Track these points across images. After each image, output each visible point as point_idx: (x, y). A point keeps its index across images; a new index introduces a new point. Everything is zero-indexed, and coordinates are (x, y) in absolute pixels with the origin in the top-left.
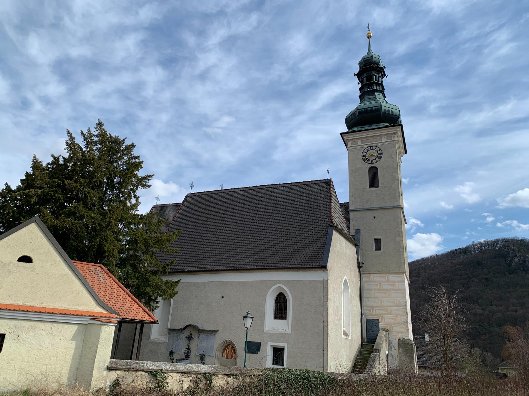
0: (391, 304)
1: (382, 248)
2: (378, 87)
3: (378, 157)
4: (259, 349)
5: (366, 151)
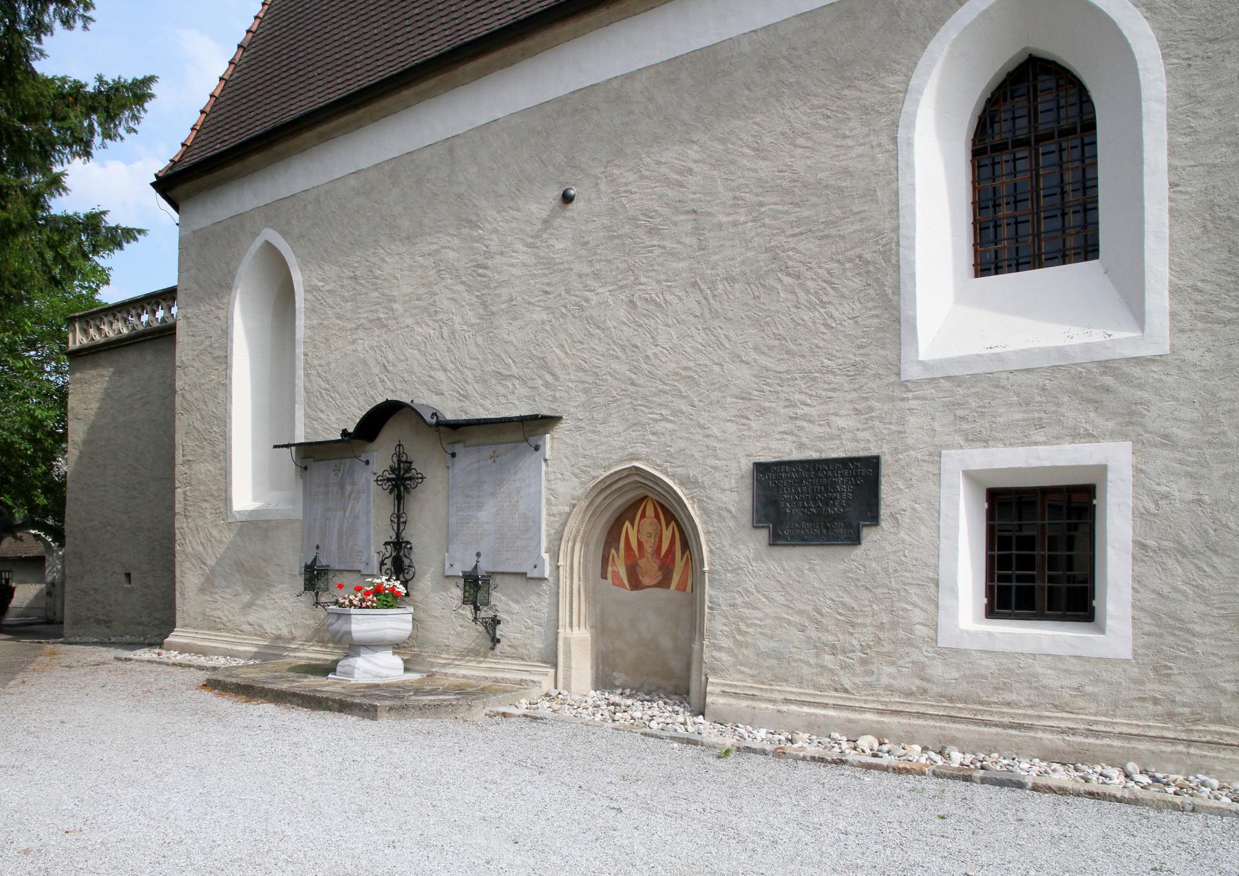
4: (869, 510)
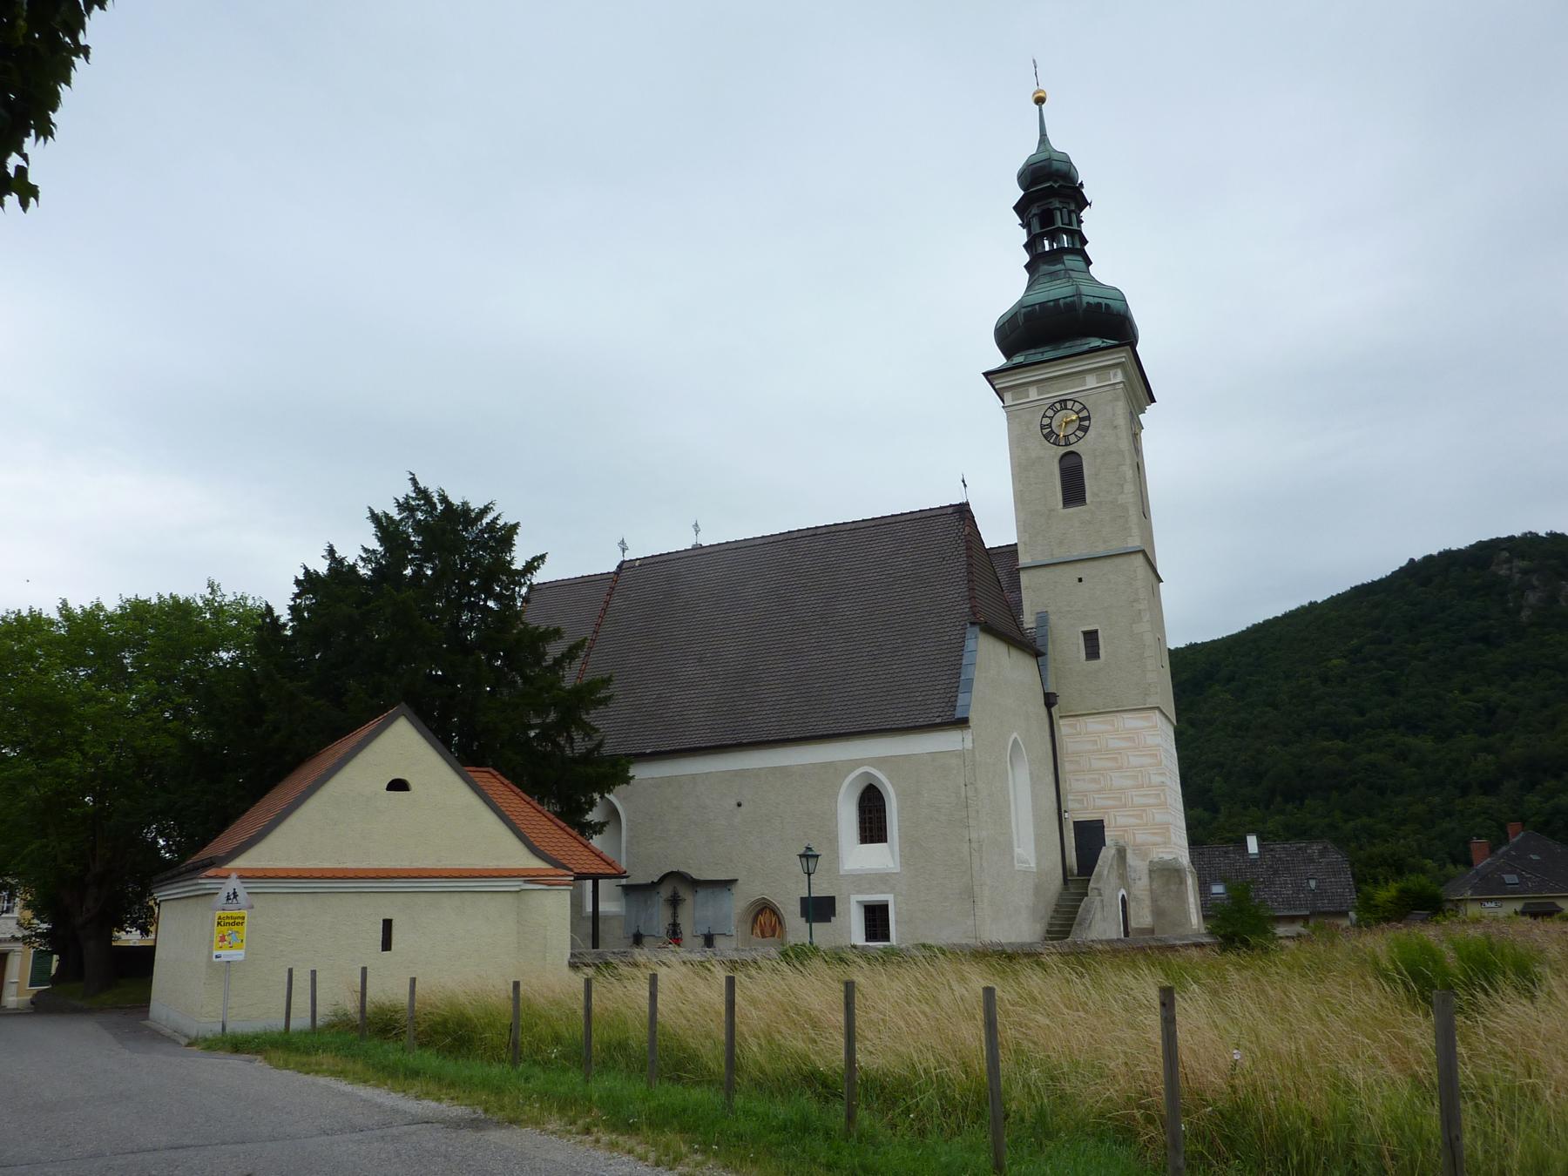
0: (1129, 783)
1: (1102, 652)
3: (1080, 428)
5: (1050, 413)
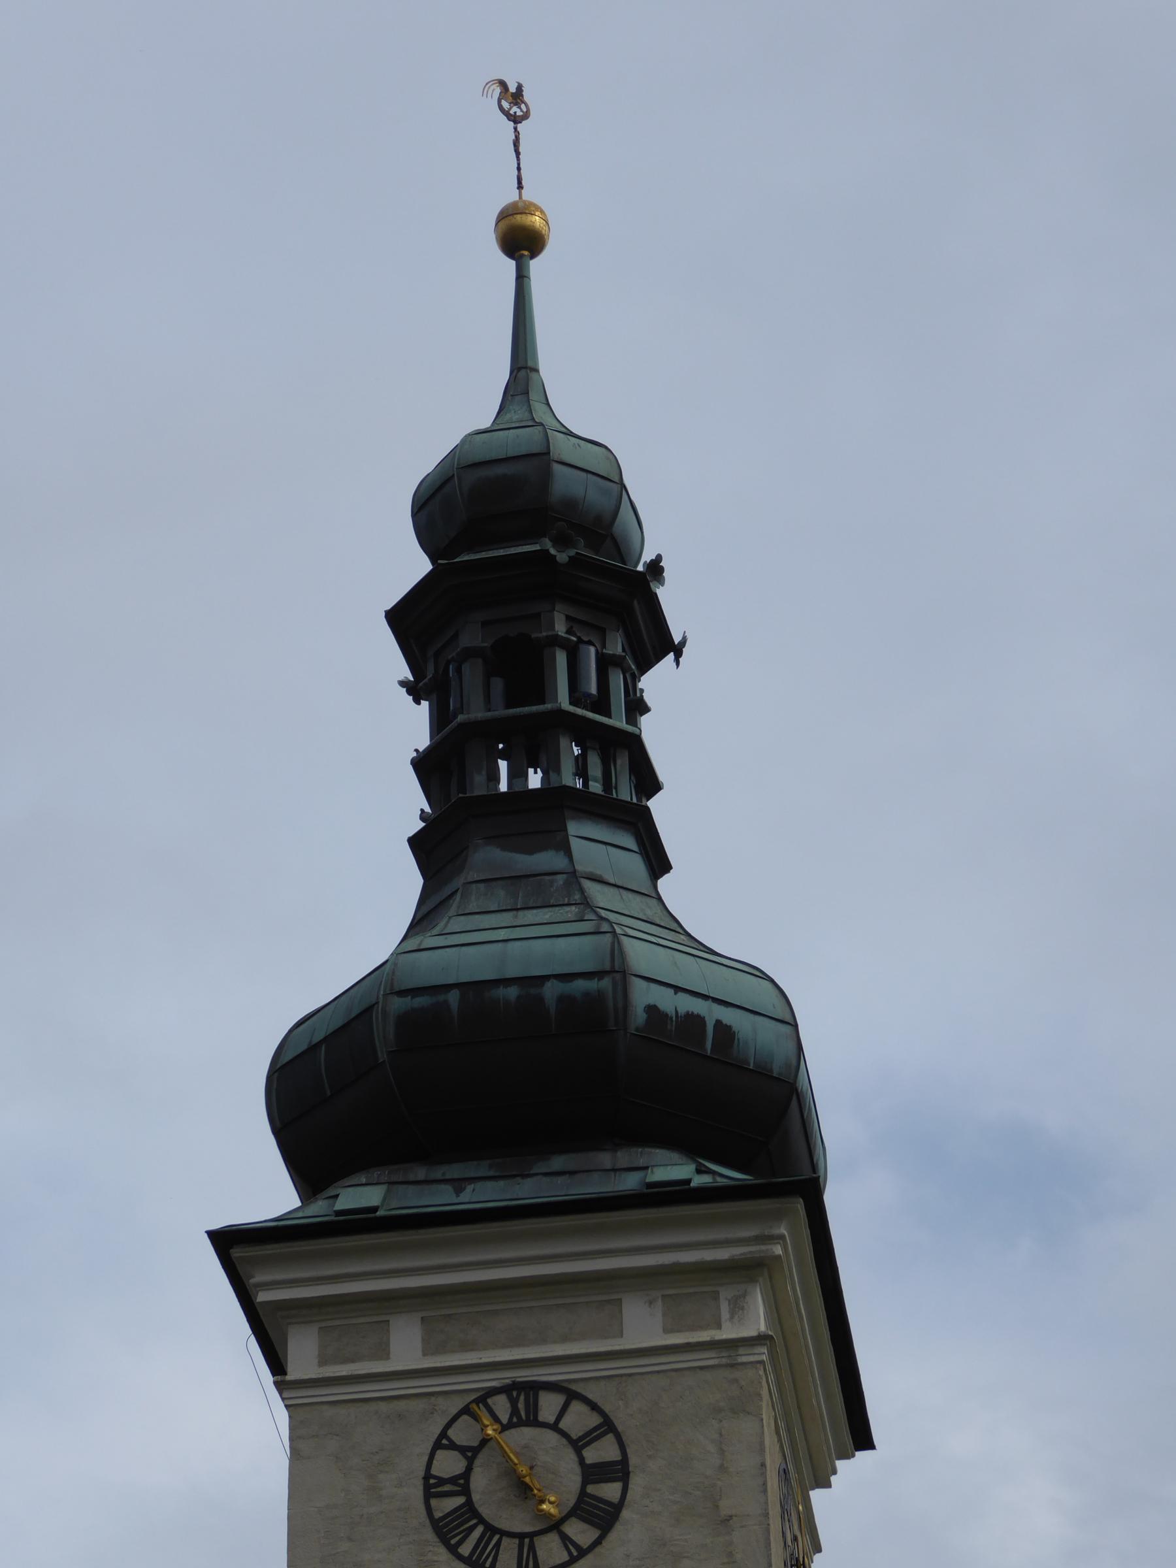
2: (595, 767)
